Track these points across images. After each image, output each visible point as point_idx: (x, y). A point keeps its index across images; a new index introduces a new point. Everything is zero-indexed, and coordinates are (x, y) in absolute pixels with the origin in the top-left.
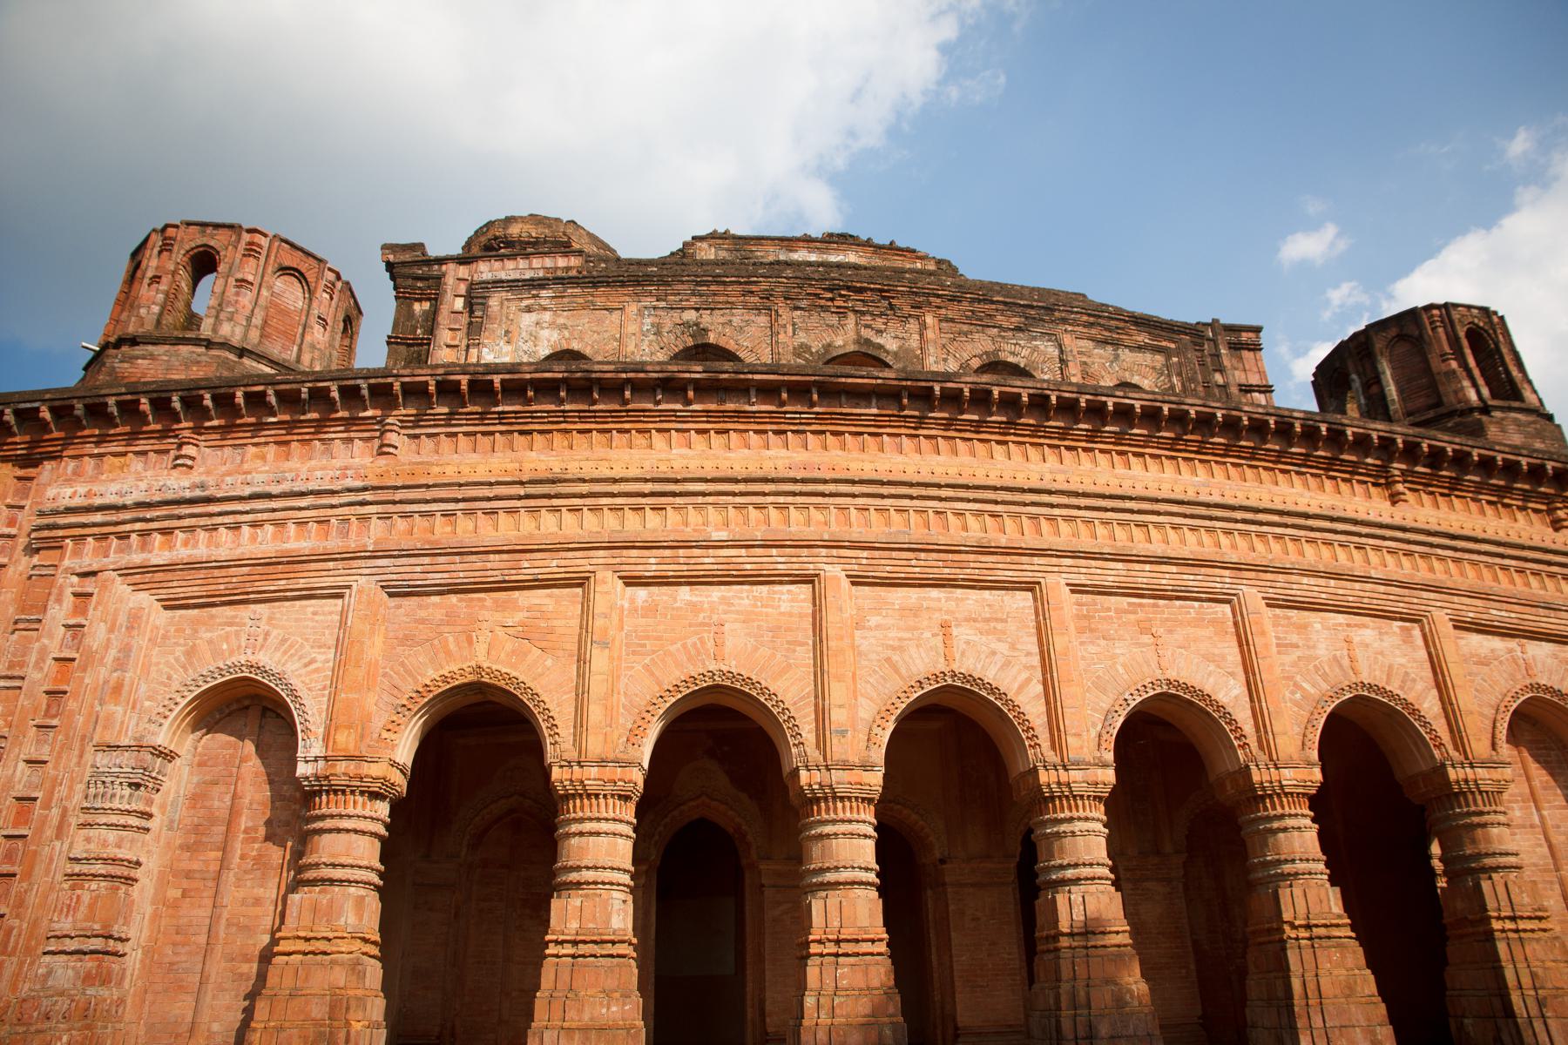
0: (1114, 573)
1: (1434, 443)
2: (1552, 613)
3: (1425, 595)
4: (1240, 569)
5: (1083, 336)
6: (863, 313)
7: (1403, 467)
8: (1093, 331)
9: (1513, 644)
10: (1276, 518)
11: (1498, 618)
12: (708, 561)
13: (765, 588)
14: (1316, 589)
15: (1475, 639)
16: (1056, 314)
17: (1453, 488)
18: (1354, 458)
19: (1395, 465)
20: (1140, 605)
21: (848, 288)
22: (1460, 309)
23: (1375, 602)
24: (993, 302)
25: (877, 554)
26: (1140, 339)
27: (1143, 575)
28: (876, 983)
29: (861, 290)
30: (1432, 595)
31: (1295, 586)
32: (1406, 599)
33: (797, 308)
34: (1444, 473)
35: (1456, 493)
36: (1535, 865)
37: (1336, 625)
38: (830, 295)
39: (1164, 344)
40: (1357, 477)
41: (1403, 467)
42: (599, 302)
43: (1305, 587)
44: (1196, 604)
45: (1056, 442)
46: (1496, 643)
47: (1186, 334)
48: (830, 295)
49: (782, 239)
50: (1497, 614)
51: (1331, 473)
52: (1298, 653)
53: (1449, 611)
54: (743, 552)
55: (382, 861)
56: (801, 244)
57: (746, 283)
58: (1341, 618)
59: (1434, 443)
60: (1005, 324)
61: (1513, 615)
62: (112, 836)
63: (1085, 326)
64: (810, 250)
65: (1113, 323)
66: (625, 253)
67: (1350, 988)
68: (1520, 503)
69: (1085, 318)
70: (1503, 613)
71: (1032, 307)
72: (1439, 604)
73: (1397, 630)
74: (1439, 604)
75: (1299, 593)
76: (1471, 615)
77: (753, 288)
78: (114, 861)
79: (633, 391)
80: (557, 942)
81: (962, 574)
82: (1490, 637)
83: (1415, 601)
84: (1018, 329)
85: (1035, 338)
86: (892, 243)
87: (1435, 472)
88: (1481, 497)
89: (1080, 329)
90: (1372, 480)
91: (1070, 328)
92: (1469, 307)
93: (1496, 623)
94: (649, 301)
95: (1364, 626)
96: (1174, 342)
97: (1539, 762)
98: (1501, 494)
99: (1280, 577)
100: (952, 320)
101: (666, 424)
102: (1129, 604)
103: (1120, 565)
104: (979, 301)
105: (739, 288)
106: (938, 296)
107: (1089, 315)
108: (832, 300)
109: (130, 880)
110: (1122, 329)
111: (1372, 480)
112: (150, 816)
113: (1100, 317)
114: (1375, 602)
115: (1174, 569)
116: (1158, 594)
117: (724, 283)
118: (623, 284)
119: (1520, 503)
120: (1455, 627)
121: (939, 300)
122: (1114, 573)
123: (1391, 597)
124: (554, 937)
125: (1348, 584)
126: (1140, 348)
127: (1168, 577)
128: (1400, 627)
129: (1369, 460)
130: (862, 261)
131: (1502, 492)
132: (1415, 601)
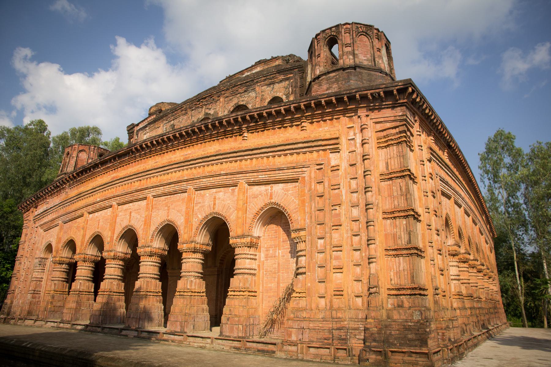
0: (161, 190)
1: (251, 114)
2: (281, 172)
3: (238, 176)
4: (188, 181)
5: (263, 85)
6: (207, 105)
7: (246, 126)
8: (266, 82)
9: (268, 187)
10: (201, 160)
11: (261, 179)
12: (97, 206)
13: (106, 210)
14: (207, 182)
15: (256, 188)
16: (255, 81)
17: (265, 127)
18: (231, 129)
19: (243, 126)
20: (167, 198)
21: (203, 99)
22: (333, 29)
23: (223, 182)
24: (237, 86)
25: (121, 197)
26: (280, 78)
27: (167, 189)
28: (104, 301)
29: (205, 98)
30: (240, 175)
31: (201, 183)
32: (232, 179)
33: (193, 110)
34: (260, 123)
35: (266, 129)
36: (271, 271)
37: (213, 193)
38: (199, 103)
39: (289, 76)
40: (234, 135)
41: (246, 126)
42: (156, 126)
43: (204, 182)
44: (179, 194)
45: (160, 153)
46: (263, 188)
47: (296, 69)
48: (199, 103)
49: (240, 72)
50: (262, 177)
51: (227, 136)
52: (200, 205)
53: (245, 180)
54: (102, 202)
55: (160, 272)
56: (245, 71)
57: (181, 108)
58: (214, 190)
59: (251, 114)
60: (241, 92)
61: (266, 176)
62: (37, 273)
63: (263, 81)
64: (248, 72)
65: (271, 76)
66: (179, 103)
67: (181, 311)
68: (290, 124)
69: (263, 78)
70: (263, 176)
71: (247, 82)
72: (242, 178)
73: (230, 191)
74: (242, 178)
75: (202, 185)
76: (252, 179)
77: (183, 109)
78: (37, 278)
79: (101, 165)
80: (231, 291)
81: (134, 198)
82: (261, 186)
83: (235, 179)
84: (245, 91)
85: (250, 92)
86: (272, 57)
87: (256, 124)
88: (275, 127)
89: (263, 83)
90: (239, 134)
91: (259, 84)
92: (330, 28)
93: (261, 181)
94: (165, 122)
95: (221, 191)
96: (292, 74)
97: (285, 231)
98: (282, 123)
99: (198, 181)
100: (228, 97)
101: (99, 174)
102: (165, 198)
103: (162, 188)
104: (234, 87)
105: (180, 110)
106: (223, 91)
107: (264, 77)
108: (199, 104)
109: (42, 281)
110: (275, 77)
111: (239, 134)
112: (44, 270)
113: (267, 76)
114: (223, 182)
115: (173, 185)
116: (171, 194)
117: (177, 110)
118: (160, 120)
119: (290, 124)
120: (249, 185)
121: (223, 92)
122: (161, 190)
123: (228, 179)
124: (231, 290)
125: (216, 178)
126: (281, 81)
127: (171, 188)
128: (232, 190)
129: (236, 128)
130: (262, 69)
131: (282, 122)
132: (235, 179)
